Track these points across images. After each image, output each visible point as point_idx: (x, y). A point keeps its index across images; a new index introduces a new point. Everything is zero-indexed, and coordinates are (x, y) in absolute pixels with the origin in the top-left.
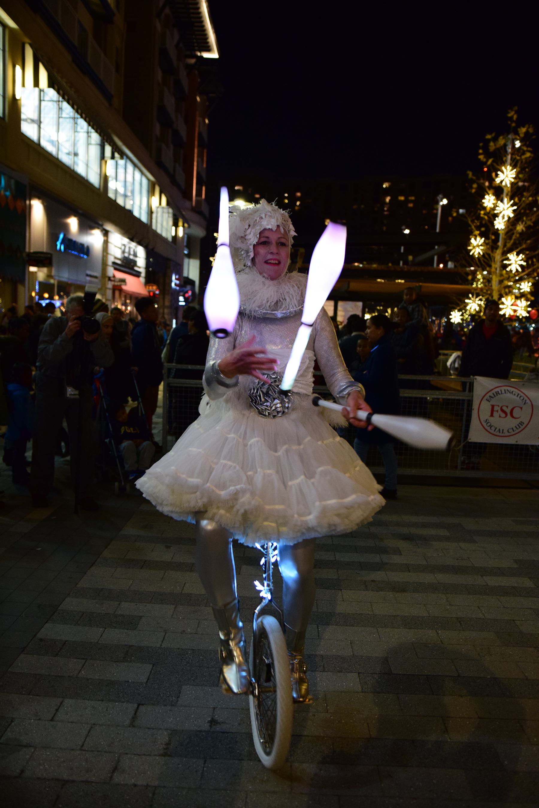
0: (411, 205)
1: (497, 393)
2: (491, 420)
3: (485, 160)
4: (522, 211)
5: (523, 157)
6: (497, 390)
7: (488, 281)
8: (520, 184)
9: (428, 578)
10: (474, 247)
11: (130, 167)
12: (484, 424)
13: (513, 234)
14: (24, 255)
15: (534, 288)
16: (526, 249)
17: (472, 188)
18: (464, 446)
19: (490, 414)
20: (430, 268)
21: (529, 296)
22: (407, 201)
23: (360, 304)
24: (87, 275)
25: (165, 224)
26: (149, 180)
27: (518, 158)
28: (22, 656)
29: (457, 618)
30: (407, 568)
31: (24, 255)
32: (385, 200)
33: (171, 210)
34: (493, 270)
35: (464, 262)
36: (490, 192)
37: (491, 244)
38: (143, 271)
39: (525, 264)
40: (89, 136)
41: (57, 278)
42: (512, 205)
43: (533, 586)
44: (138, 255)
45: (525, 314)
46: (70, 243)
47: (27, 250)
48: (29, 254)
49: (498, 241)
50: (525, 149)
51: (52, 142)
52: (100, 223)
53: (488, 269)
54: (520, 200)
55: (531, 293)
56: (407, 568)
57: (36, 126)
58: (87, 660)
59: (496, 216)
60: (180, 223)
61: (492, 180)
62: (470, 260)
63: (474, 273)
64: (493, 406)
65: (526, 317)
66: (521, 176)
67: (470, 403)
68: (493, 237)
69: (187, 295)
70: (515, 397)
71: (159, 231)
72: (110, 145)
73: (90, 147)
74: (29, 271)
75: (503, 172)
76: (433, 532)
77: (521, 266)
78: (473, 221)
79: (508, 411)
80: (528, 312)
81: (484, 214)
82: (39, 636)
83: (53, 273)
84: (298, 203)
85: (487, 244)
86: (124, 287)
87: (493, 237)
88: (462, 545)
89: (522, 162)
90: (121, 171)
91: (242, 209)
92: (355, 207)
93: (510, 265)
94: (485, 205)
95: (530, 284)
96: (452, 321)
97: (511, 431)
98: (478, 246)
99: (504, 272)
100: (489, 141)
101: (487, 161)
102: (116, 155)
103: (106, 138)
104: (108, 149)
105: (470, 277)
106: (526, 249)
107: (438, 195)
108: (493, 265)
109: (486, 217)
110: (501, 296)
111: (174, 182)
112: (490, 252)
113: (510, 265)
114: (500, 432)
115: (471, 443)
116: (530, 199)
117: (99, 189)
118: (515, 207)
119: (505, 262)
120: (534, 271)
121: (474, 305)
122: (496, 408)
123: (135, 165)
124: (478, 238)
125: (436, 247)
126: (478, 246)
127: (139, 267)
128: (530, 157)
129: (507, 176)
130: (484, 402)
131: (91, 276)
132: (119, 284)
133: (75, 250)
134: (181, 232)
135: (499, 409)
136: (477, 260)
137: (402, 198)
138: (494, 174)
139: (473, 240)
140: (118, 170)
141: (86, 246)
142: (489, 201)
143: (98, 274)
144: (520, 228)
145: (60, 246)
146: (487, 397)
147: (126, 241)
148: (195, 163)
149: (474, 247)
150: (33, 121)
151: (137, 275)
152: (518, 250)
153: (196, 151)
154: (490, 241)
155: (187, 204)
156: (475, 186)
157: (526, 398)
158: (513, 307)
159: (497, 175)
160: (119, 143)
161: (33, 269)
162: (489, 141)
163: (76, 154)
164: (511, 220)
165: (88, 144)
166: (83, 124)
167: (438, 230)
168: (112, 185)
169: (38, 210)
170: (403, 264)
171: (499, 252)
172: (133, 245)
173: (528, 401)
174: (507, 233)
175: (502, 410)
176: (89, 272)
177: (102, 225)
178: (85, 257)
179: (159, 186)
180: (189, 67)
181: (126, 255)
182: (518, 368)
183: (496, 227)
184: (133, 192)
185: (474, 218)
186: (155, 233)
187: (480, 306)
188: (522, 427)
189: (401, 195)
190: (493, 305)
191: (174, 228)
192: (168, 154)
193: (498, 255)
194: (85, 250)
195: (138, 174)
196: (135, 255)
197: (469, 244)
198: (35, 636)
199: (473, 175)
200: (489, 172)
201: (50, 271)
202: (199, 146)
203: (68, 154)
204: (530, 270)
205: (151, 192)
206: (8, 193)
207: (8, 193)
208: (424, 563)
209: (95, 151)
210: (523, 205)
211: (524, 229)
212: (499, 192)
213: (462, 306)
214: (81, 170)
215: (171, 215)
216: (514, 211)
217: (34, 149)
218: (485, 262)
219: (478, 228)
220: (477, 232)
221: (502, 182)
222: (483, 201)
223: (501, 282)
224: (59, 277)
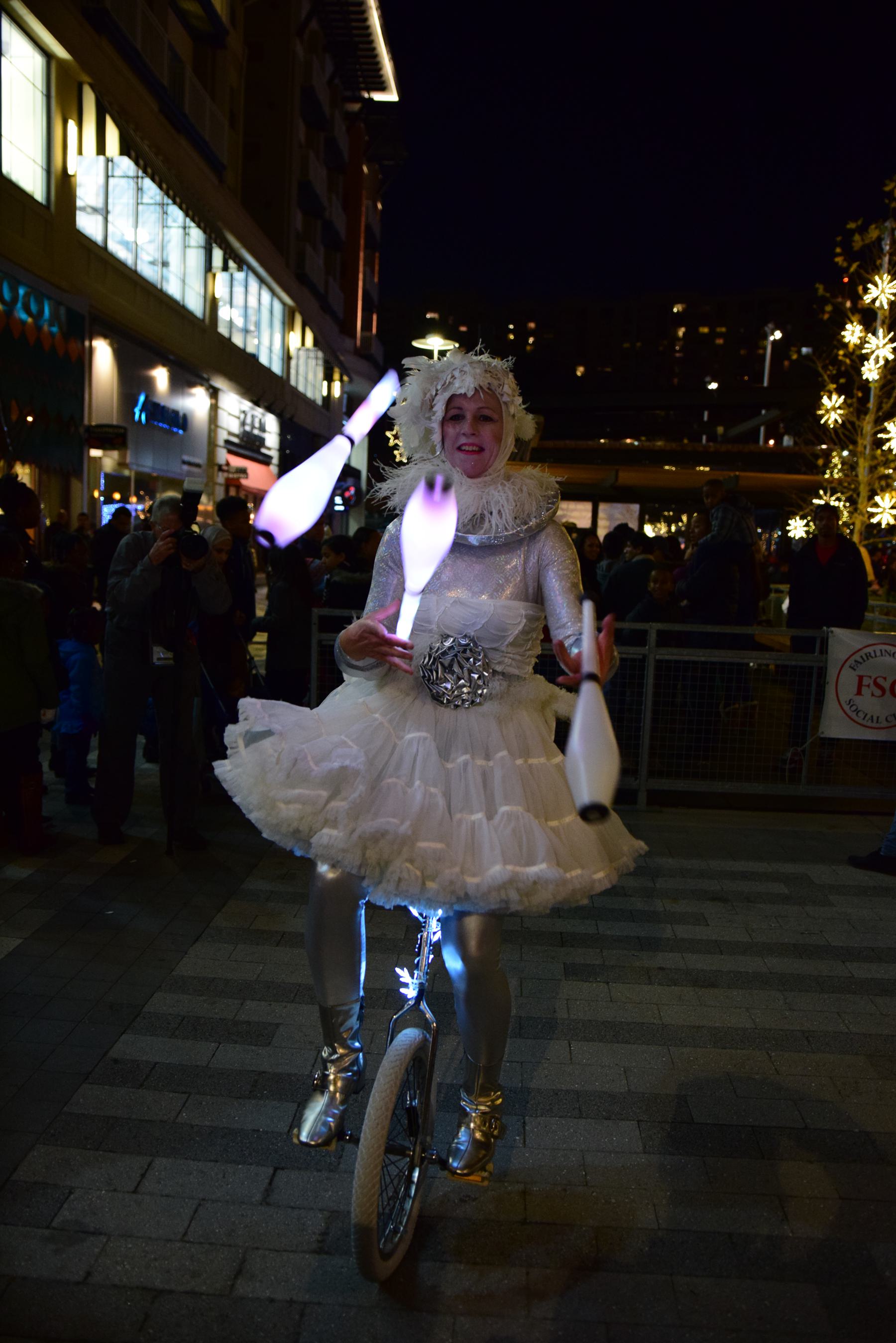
0: (720, 341)
1: (868, 656)
2: (858, 700)
3: (845, 265)
7: (850, 466)
10: (827, 411)
12: (846, 708)
17: (823, 312)
19: (855, 690)
22: (713, 335)
23: (636, 507)
24: (184, 462)
25: (311, 376)
26: (284, 304)
30: (717, 947)
31: (82, 430)
32: (676, 333)
33: (320, 354)
34: (860, 448)
36: (855, 318)
38: (274, 454)
40: (186, 234)
44: (267, 428)
46: (156, 410)
47: (86, 422)
48: (89, 429)
49: (868, 401)
51: (125, 244)
52: (205, 376)
56: (717, 947)
57: (100, 219)
58: (190, 1094)
59: (865, 358)
60: (336, 376)
61: (857, 298)
63: (827, 455)
64: (861, 678)
69: (347, 495)
71: (301, 388)
72: (221, 248)
73: (188, 251)
75: (876, 285)
78: (825, 368)
81: (845, 355)
83: (128, 460)
84: (531, 340)
85: (849, 406)
86: (244, 482)
87: (860, 394)
90: (239, 290)
93: (888, 440)
98: (834, 409)
100: (852, 232)
102: (231, 264)
104: (218, 255)
105: (820, 462)
107: (766, 324)
108: (860, 441)
109: (848, 361)
111: (326, 308)
112: (854, 419)
113: (888, 440)
122: (866, 681)
123: (262, 281)
124: (835, 397)
126: (834, 409)
127: (269, 449)
130: (846, 671)
131: (190, 464)
132: (235, 476)
134: (337, 391)
137: (705, 330)
138: (860, 288)
139: (825, 400)
141: (181, 414)
142: (852, 333)
146: (851, 661)
147: (247, 405)
148: (361, 276)
149: (827, 411)
150: (95, 210)
151: (266, 461)
153: (362, 255)
155: (348, 342)
156: (829, 308)
159: (866, 290)
160: (236, 244)
161: (95, 453)
162: (852, 232)
163: (165, 264)
164: (889, 366)
165: (185, 247)
166: (176, 214)
167: (766, 384)
168: (224, 313)
169: (103, 356)
170: (708, 440)
171: (869, 418)
172: (259, 411)
174: (882, 387)
176: (186, 458)
177: (208, 380)
178: (181, 432)
180: (350, 118)
181: (248, 428)
183: (864, 377)
184: (258, 324)
186: (295, 392)
189: (704, 325)
191: (325, 383)
193: (867, 425)
194: (181, 421)
195: (266, 296)
196: (262, 429)
197: (819, 405)
199: (825, 290)
200: (853, 285)
201: (123, 456)
202: (366, 247)
203: (153, 263)
205: (288, 324)
206: (55, 329)
207: (55, 329)
209: (196, 257)
212: (869, 319)
214: (173, 289)
215: (320, 362)
217: (98, 256)
218: (845, 435)
219: (834, 379)
220: (832, 386)
221: (874, 301)
223: (873, 469)
224: (138, 465)
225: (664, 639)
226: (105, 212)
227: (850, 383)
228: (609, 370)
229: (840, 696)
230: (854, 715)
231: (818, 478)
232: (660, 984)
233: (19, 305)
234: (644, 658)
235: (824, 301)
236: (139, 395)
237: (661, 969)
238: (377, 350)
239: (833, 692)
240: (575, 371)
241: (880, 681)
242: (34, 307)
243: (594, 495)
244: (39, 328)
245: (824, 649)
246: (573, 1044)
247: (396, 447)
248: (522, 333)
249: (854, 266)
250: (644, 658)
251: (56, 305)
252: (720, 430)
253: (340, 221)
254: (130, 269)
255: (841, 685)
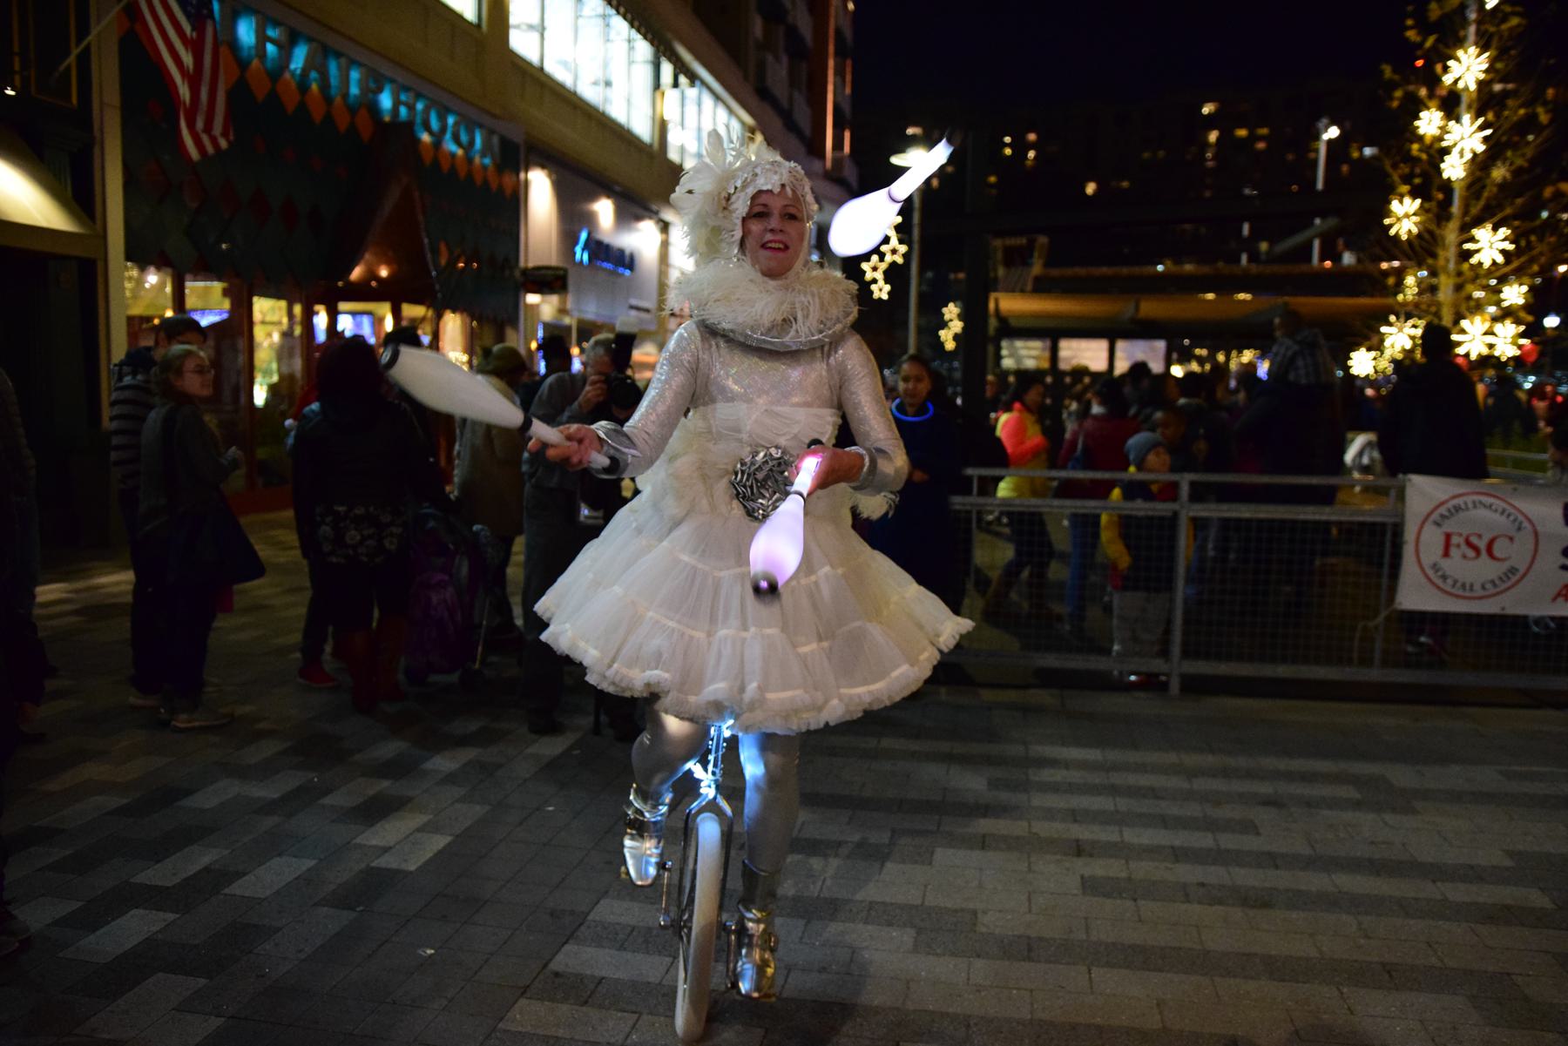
0: (1261, 145)
1: (1457, 509)
2: (1446, 564)
4: (1504, 139)
5: (1504, 27)
6: (1455, 502)
7: (1428, 289)
8: (1497, 87)
9: (1315, 882)
10: (1399, 219)
11: (708, 100)
12: (1430, 573)
13: (1484, 187)
14: (517, 274)
15: (1535, 296)
16: (1515, 217)
18: (1388, 619)
19: (1440, 551)
20: (1304, 268)
21: (1522, 314)
22: (1253, 138)
23: (1161, 345)
24: (632, 307)
26: (743, 123)
27: (1492, 29)
28: (523, 1002)
29: (1383, 965)
30: (1272, 860)
31: (517, 274)
34: (1441, 262)
35: (1377, 250)
36: (1433, 104)
37: (1435, 210)
39: (1511, 247)
40: (631, 49)
41: (576, 314)
42: (1481, 128)
43: (1549, 905)
45: (1513, 352)
46: (601, 251)
47: (522, 264)
48: (525, 272)
50: (1508, 9)
51: (565, 64)
52: (654, 207)
53: (1430, 261)
54: (1498, 116)
55: (1527, 307)
56: (1272, 860)
57: (536, 36)
58: (641, 1014)
61: (1434, 81)
62: (1393, 246)
63: (1400, 274)
64: (1448, 537)
65: (1515, 358)
66: (1499, 65)
67: (1398, 530)
68: (1440, 196)
70: (1496, 516)
72: (670, 61)
73: (634, 67)
74: (527, 306)
75: (1458, 60)
76: (1326, 791)
77: (1503, 252)
79: (1482, 545)
80: (1520, 347)
81: (1420, 150)
82: (553, 966)
83: (569, 305)
84: (1031, 154)
85: (1427, 211)
88: (1389, 817)
89: (1501, 37)
90: (691, 109)
91: (865, 515)
92: (1146, 155)
93: (1477, 251)
94: (1421, 131)
95: (1525, 288)
96: (1354, 371)
97: (1488, 586)
98: (1407, 216)
99: (1465, 266)
101: (1425, 40)
102: (683, 79)
103: (663, 49)
104: (667, 69)
106: (1515, 217)
107: (1318, 118)
108: (1441, 253)
109: (1424, 156)
110: (1459, 317)
111: (791, 125)
112: (1433, 227)
113: (1477, 251)
114: (1464, 589)
115: (1403, 612)
116: (1522, 111)
117: (651, 146)
118: (1488, 132)
119: (1467, 246)
120: (1532, 261)
121: (1400, 338)
122: (1455, 540)
123: (717, 97)
124: (1407, 200)
125: (1318, 221)
126: (1407, 216)
128: (1518, 26)
129: (1468, 68)
130: (1429, 529)
131: (638, 309)
133: (608, 261)
135: (1461, 540)
136: (1406, 247)
138: (1439, 68)
139: (1395, 206)
140: (687, 109)
141: (627, 253)
142: (1429, 122)
143: (649, 304)
144: (1499, 173)
145: (581, 255)
146: (1435, 516)
148: (830, 88)
150: (531, 27)
152: (1496, 219)
153: (831, 63)
154: (1433, 204)
156: (1398, 94)
157: (1521, 518)
158: (1485, 337)
159: (1446, 69)
160: (687, 56)
161: (532, 299)
163: (608, 84)
164: (1478, 160)
165: (631, 63)
166: (620, 25)
168: (675, 138)
169: (540, 189)
170: (1250, 260)
173: (1526, 524)
175: (1469, 544)
176: (634, 302)
177: (657, 213)
178: (627, 273)
179: (763, 133)
182: (1501, 462)
183: (1445, 176)
185: (1398, 158)
187: (1413, 338)
188: (1514, 579)
189: (1241, 127)
190: (1437, 340)
192: (778, 74)
193: (1451, 234)
194: (625, 261)
195: (722, 113)
197: (1388, 214)
198: (545, 966)
199: (1394, 71)
200: (1429, 66)
201: (563, 302)
202: (837, 54)
203: (595, 83)
204: (1523, 259)
206: (487, 161)
207: (487, 161)
208: (1307, 851)
209: (644, 73)
210: (1506, 126)
211: (1508, 176)
212: (1451, 105)
213: (1375, 340)
214: (617, 112)
216: (1486, 140)
217: (533, 78)
218: (1421, 249)
219: (1406, 179)
220: (1405, 188)
221: (1456, 82)
222: (1417, 123)
223: (1459, 288)
224: (580, 311)
225: (1200, 493)
226: (542, 30)
227: (1428, 185)
228: (1125, 184)
229: (1422, 556)
230: (1439, 582)
231: (1390, 301)
232: (1200, 903)
233: (448, 136)
234: (1176, 515)
235: (1393, 86)
236: (579, 232)
237: (1202, 885)
238: (850, 173)
239: (1414, 559)
240: (1083, 188)
241: (1474, 540)
242: (464, 138)
243: (1111, 332)
244: (469, 160)
245: (1401, 496)
246: (1095, 971)
247: (875, 281)
248: (1020, 147)
249: (1429, 43)
250: (1176, 515)
251: (489, 133)
252: (1264, 246)
253: (803, 22)
254: (569, 91)
255: (1422, 546)
